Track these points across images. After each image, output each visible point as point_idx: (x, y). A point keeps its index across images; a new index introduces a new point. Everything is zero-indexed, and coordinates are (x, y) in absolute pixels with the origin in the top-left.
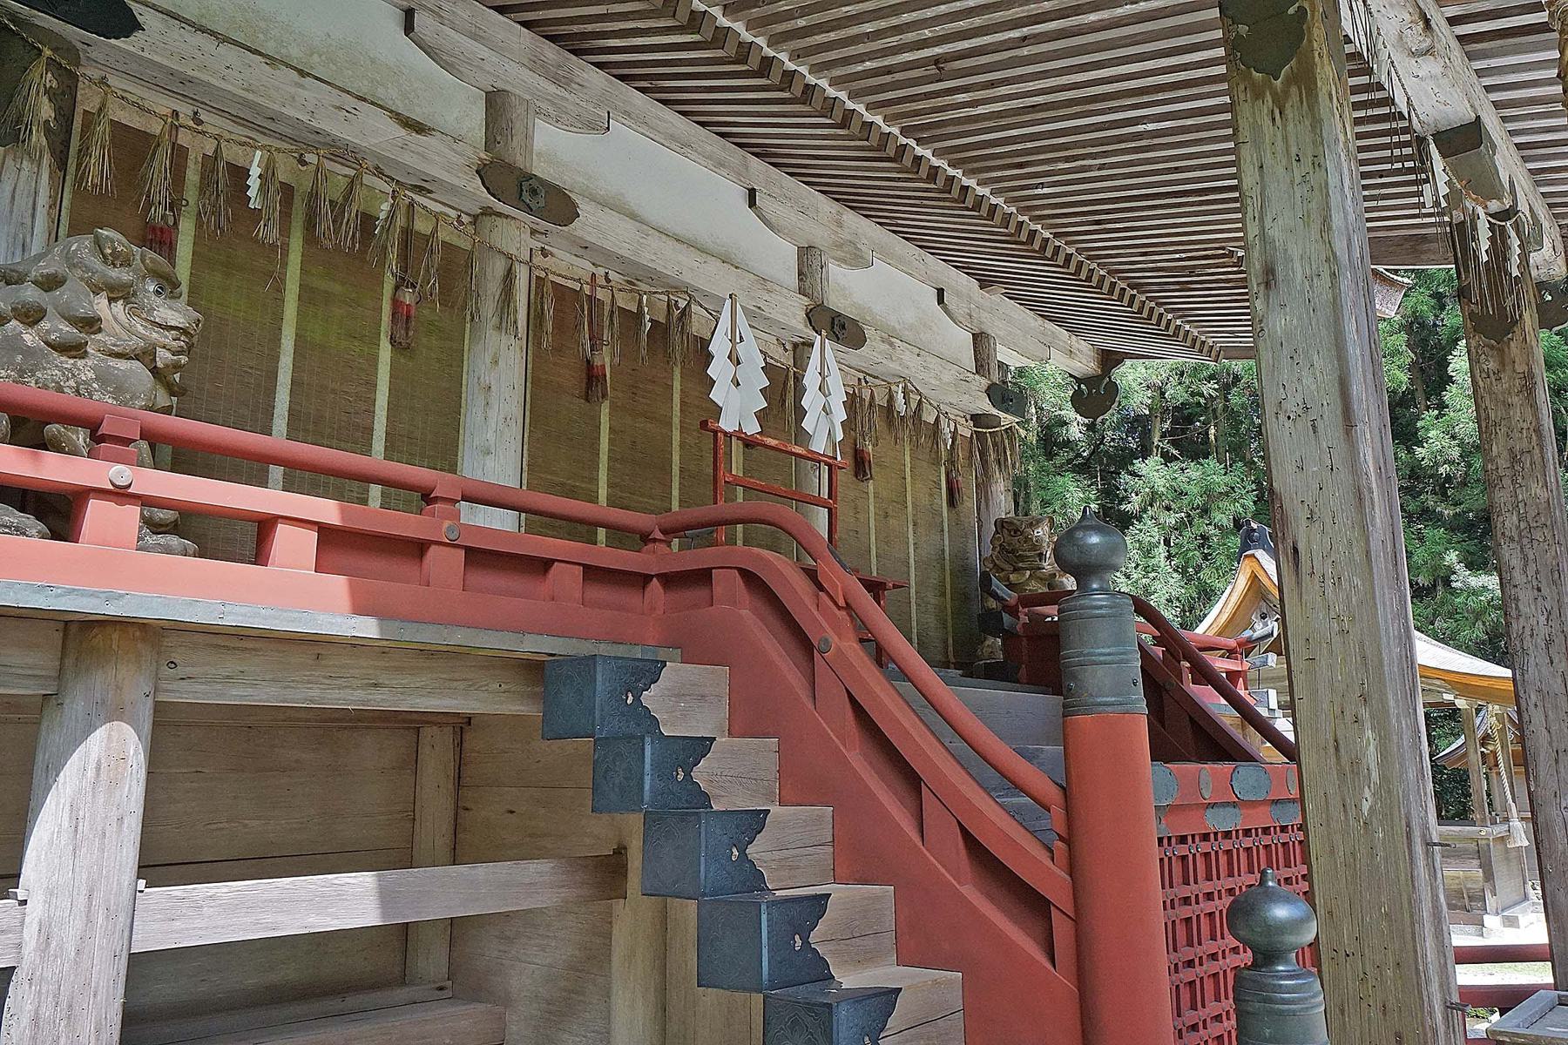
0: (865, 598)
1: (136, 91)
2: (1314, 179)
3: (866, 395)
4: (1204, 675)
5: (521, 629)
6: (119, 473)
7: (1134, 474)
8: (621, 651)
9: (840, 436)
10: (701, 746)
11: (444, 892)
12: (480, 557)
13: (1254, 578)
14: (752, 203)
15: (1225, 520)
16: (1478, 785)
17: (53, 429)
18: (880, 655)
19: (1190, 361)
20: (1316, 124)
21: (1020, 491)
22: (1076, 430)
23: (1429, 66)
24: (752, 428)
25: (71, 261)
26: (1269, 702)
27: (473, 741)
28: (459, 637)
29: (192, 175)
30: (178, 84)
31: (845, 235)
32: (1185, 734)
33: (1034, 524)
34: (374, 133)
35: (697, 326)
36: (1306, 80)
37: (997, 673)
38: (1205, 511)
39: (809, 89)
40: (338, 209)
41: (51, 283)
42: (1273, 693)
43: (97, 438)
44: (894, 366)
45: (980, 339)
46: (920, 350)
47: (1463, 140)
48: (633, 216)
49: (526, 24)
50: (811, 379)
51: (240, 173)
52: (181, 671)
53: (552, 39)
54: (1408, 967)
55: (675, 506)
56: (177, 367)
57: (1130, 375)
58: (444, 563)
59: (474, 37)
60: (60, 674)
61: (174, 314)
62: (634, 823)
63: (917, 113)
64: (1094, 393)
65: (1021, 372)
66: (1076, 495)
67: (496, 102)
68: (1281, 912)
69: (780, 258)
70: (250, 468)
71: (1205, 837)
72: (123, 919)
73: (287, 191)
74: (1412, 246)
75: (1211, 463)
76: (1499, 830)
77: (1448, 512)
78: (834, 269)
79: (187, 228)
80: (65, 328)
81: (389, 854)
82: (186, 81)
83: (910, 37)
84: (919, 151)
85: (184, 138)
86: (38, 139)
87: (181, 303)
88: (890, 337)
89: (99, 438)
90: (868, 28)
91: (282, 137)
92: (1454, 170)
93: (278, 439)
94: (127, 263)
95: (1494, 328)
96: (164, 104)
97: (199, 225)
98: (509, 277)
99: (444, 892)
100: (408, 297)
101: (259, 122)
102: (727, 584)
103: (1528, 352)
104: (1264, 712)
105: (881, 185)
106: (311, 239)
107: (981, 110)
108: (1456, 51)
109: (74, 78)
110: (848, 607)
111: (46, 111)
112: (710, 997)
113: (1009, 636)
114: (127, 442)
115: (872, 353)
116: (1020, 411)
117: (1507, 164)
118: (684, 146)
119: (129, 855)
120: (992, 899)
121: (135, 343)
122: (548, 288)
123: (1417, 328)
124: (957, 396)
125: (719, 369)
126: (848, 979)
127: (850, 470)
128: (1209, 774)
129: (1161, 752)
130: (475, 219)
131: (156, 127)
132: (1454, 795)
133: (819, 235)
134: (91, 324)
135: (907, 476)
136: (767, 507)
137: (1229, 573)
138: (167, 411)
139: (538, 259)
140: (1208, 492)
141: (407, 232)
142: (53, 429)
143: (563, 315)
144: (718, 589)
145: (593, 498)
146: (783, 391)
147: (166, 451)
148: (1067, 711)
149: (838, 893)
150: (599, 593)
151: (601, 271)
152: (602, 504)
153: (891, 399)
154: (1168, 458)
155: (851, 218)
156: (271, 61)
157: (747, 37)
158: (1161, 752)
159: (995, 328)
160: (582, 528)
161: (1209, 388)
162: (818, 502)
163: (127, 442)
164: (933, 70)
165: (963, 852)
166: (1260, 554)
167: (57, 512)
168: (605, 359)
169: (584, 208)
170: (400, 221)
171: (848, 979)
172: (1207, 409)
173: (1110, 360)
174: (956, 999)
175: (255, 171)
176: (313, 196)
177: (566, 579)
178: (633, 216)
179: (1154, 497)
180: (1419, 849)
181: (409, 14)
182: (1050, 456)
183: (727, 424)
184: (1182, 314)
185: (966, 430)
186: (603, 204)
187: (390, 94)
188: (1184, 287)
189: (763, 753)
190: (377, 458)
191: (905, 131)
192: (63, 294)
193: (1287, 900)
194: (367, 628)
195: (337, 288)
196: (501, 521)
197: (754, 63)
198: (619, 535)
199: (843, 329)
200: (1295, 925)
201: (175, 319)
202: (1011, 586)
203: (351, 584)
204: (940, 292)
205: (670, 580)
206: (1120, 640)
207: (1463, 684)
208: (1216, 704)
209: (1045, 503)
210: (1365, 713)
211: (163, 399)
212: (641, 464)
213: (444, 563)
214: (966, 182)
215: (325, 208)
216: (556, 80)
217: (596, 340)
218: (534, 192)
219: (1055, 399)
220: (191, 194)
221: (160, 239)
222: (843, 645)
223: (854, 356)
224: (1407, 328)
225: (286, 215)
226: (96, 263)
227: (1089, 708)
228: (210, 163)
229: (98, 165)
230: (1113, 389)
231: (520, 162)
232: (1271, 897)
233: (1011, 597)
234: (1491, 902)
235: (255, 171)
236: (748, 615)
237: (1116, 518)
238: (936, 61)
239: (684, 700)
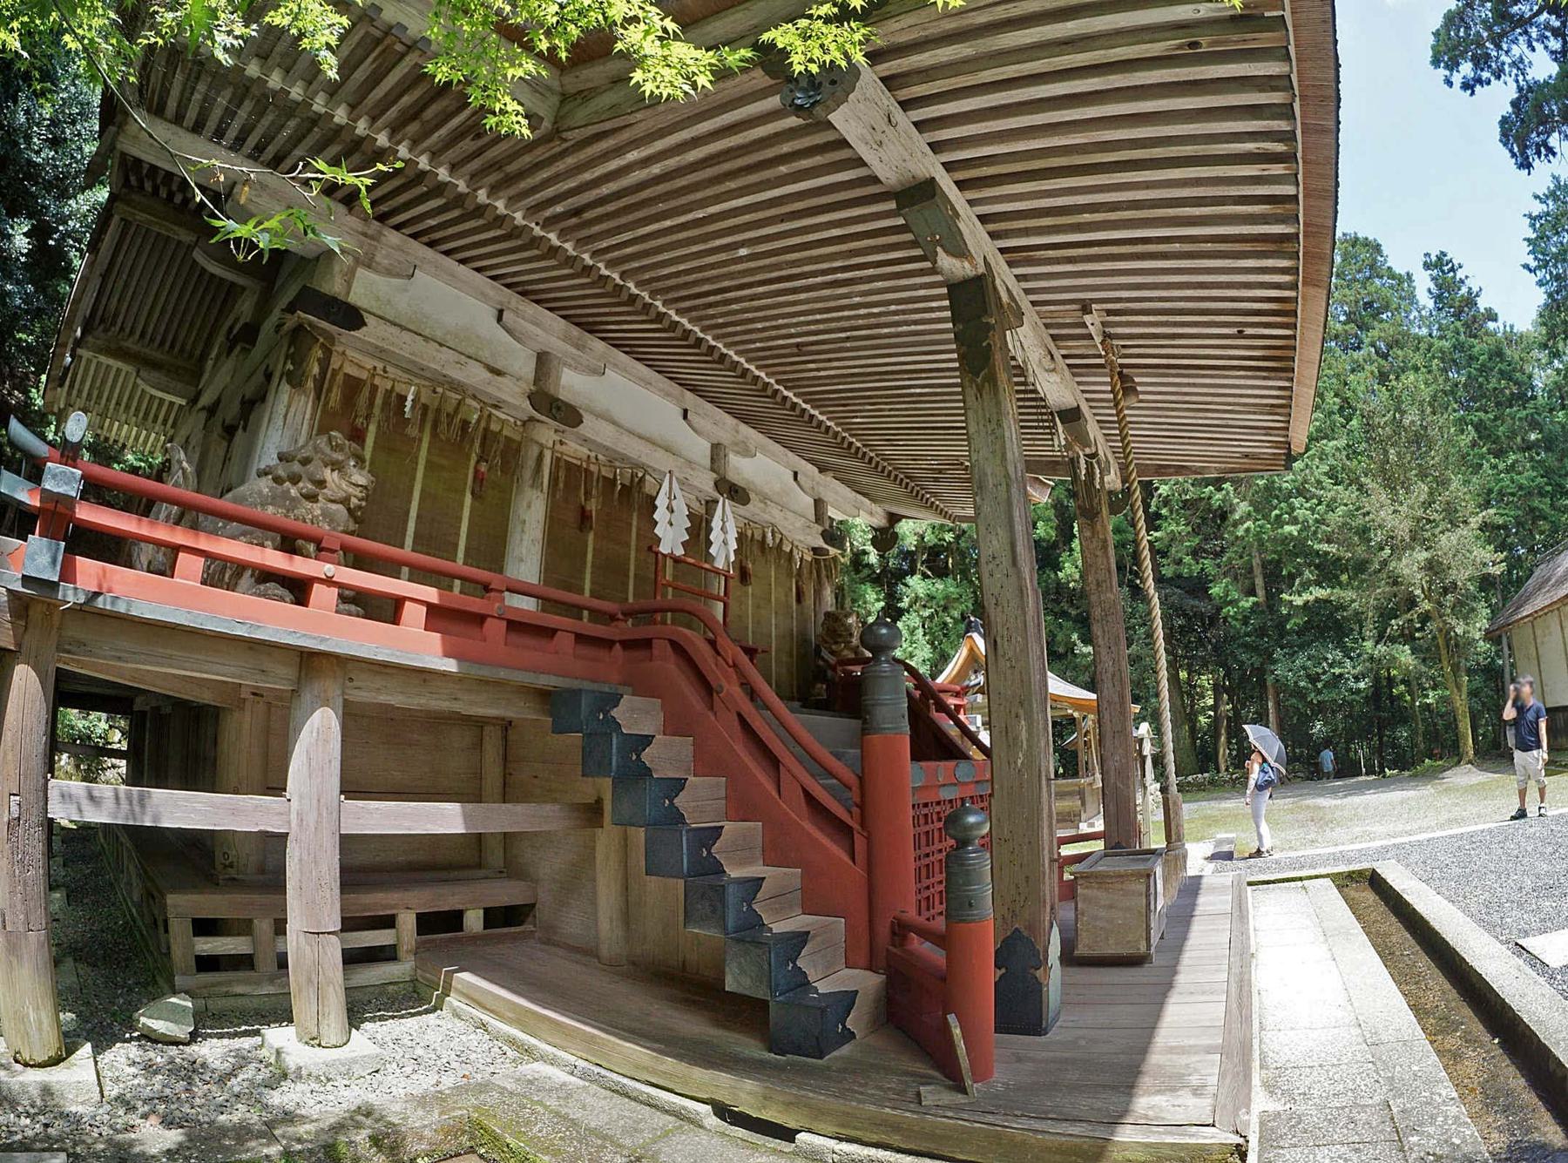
0: (744, 659)
1: (358, 356)
2: (998, 432)
3: (749, 533)
4: (941, 707)
5: (537, 670)
6: (328, 569)
7: (906, 585)
8: (595, 687)
9: (732, 558)
10: (647, 740)
11: (500, 818)
12: (516, 626)
13: (971, 650)
14: (685, 417)
15: (956, 614)
16: (1082, 758)
17: (300, 542)
18: (753, 694)
19: (938, 521)
20: (998, 403)
21: (839, 594)
22: (873, 558)
23: (1054, 378)
24: (680, 552)
25: (316, 449)
26: (976, 722)
27: (512, 736)
28: (503, 674)
29: (379, 401)
30: (379, 353)
31: (740, 437)
32: (933, 744)
33: (847, 616)
34: (474, 375)
35: (649, 488)
36: (992, 380)
37: (822, 706)
38: (945, 609)
39: (723, 356)
40: (450, 417)
41: (305, 462)
42: (979, 718)
43: (319, 549)
44: (767, 517)
45: (819, 504)
46: (783, 507)
47: (1071, 416)
48: (614, 423)
49: (563, 317)
50: (716, 523)
51: (403, 399)
52: (355, 683)
53: (577, 324)
54: (1034, 845)
55: (631, 600)
56: (360, 507)
57: (906, 528)
58: (495, 628)
59: (537, 325)
60: (299, 678)
61: (361, 478)
62: (606, 784)
63: (785, 373)
64: (885, 537)
65: (841, 522)
66: (873, 601)
67: (542, 359)
68: (972, 819)
69: (700, 449)
70: (389, 567)
71: (938, 803)
72: (335, 815)
73: (425, 408)
74: (1051, 466)
75: (950, 580)
76: (1089, 780)
77: (1074, 613)
78: (731, 456)
79: (372, 428)
80: (310, 486)
81: (467, 794)
82: (382, 350)
83: (784, 332)
84: (786, 393)
85: (377, 381)
86: (310, 384)
87: (365, 472)
88: (765, 499)
89: (322, 550)
90: (759, 326)
91: (426, 379)
92: (1067, 431)
93: (407, 552)
94: (342, 450)
95: (1091, 515)
96: (369, 363)
97: (379, 427)
98: (540, 457)
99: (500, 818)
100: (483, 467)
101: (415, 371)
102: (661, 648)
103: (1104, 527)
104: (973, 728)
105: (762, 411)
106: (434, 435)
107: (822, 373)
108: (1067, 371)
109: (331, 352)
110: (735, 665)
111: (316, 370)
112: (653, 882)
113: (831, 685)
114: (333, 551)
115: (754, 509)
116: (841, 547)
117: (1093, 431)
118: (647, 384)
119: (335, 782)
121: (341, 494)
122: (562, 464)
123: (1058, 506)
124: (803, 537)
125: (660, 515)
126: (734, 873)
127: (737, 579)
128: (943, 768)
129: (916, 757)
130: (524, 423)
131: (364, 375)
132: (1070, 763)
133: (725, 437)
134: (321, 484)
135: (773, 585)
136: (689, 602)
137: (956, 648)
138: (352, 533)
139: (558, 447)
140: (947, 597)
141: (486, 429)
142: (300, 542)
143: (570, 479)
144: (655, 652)
145: (581, 591)
146: (699, 528)
147: (351, 557)
148: (865, 731)
149: (728, 826)
150: (585, 651)
151: (593, 454)
152: (586, 597)
153: (764, 536)
154: (925, 576)
155: (744, 428)
156: (426, 339)
157: (689, 326)
158: (916, 757)
159: (827, 496)
160: (575, 610)
161: (949, 537)
162: (718, 599)
163: (333, 551)
164: (795, 350)
165: (804, 804)
166: (975, 636)
167: (299, 589)
168: (593, 506)
169: (587, 418)
170: (483, 424)
171: (734, 873)
172: (948, 548)
173: (894, 518)
174: (797, 883)
175: (410, 397)
176: (438, 411)
177: (565, 642)
178: (614, 423)
179: (917, 599)
180: (1044, 782)
181: (501, 312)
182: (857, 572)
183: (664, 549)
184: (934, 494)
185: (808, 557)
186: (599, 416)
187: (485, 355)
188: (936, 480)
189: (684, 746)
190: (459, 563)
191: (778, 382)
192: (310, 467)
193: (976, 813)
194: (451, 665)
195: (444, 462)
196: (527, 604)
197: (691, 341)
198: (597, 615)
199: (736, 493)
200: (978, 825)
201: (362, 480)
202: (832, 653)
203: (443, 640)
204: (796, 474)
205: (627, 645)
206: (896, 691)
207: (1077, 704)
208: (949, 726)
209: (854, 601)
210: (1021, 712)
211: (352, 526)
212: (612, 569)
213: (495, 628)
214: (813, 412)
215: (443, 418)
216: (577, 347)
217: (588, 494)
218: (559, 409)
219: (861, 538)
220: (377, 411)
221: (357, 436)
222: (732, 689)
223: (741, 510)
224: (1054, 506)
225: (423, 421)
226: (327, 450)
227: (878, 730)
228: (388, 393)
229: (336, 396)
230: (895, 536)
231: (552, 392)
232: (969, 812)
233: (832, 660)
234: (1083, 816)
235: (410, 397)
236: (667, 666)
237: (893, 612)
238: (798, 345)
239: (635, 715)
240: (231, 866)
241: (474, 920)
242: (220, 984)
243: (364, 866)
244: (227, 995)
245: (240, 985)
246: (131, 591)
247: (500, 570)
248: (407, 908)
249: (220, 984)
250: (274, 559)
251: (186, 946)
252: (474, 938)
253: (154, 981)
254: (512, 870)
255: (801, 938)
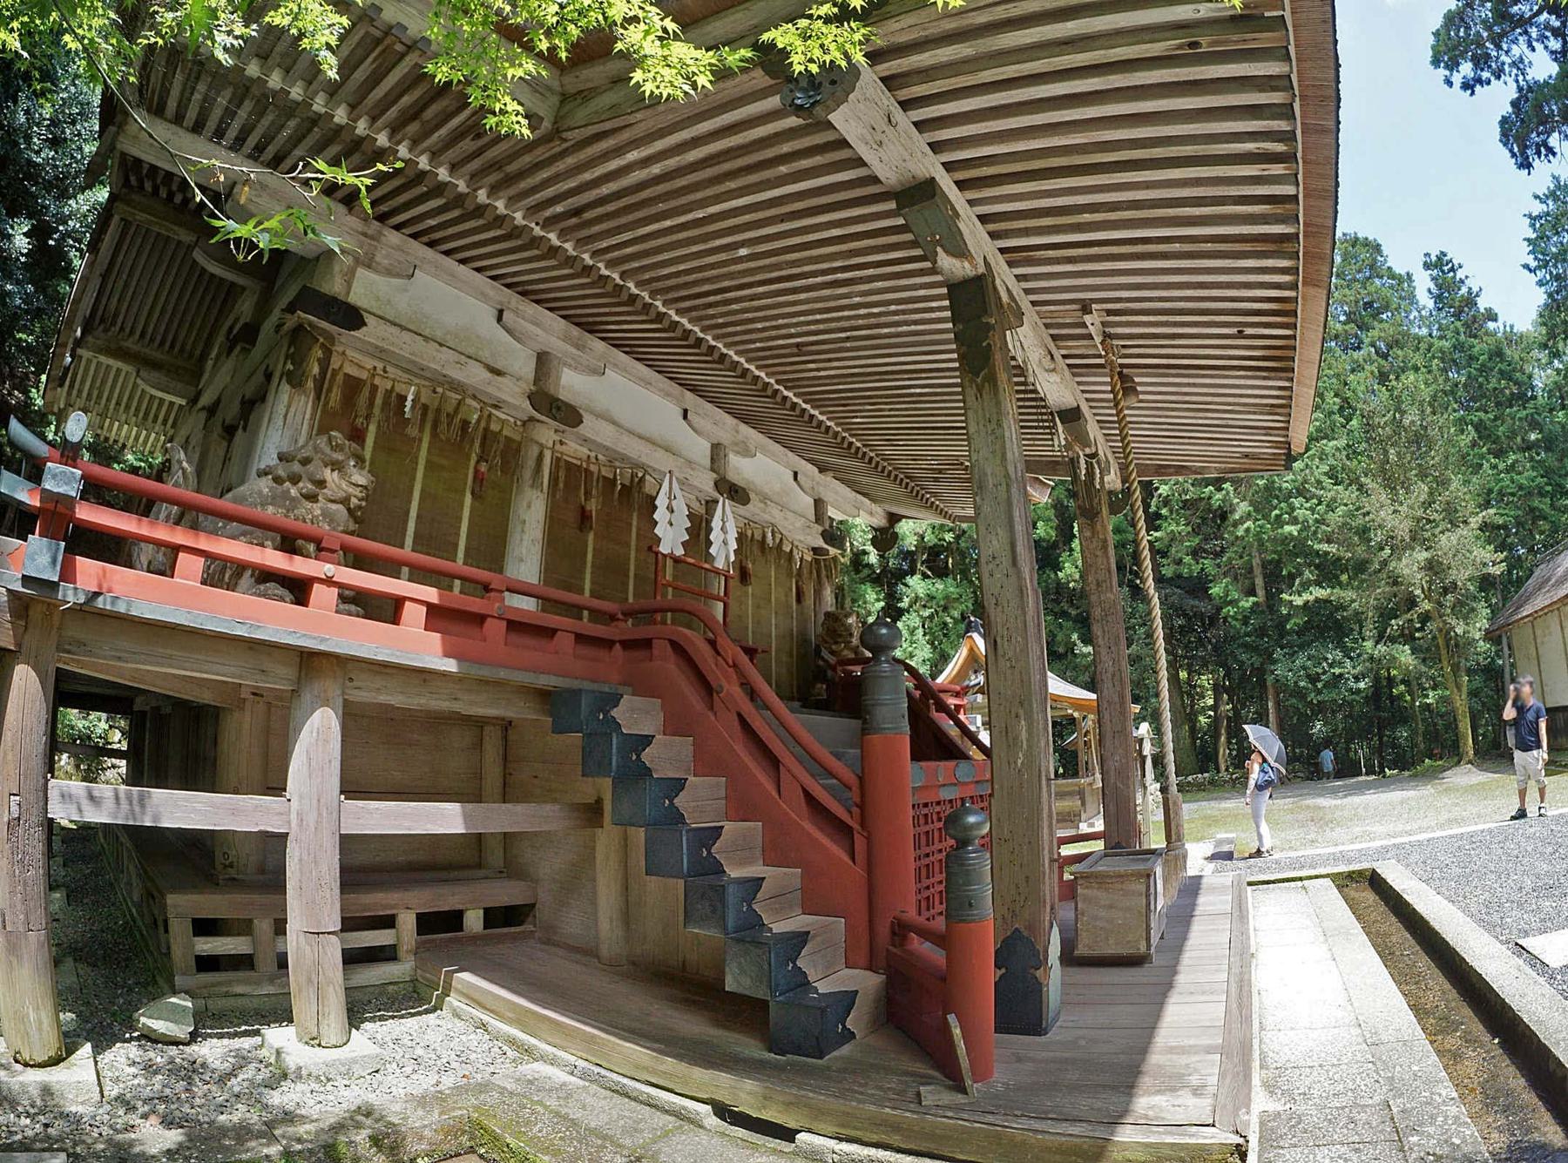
0: (744, 659)
1: (358, 356)
2: (998, 432)
3: (749, 533)
4: (941, 707)
5: (537, 670)
6: (328, 569)
7: (906, 585)
8: (595, 687)
9: (732, 558)
10: (647, 740)
11: (500, 818)
12: (516, 626)
13: (971, 650)
14: (685, 417)
15: (956, 614)
16: (1082, 758)
17: (300, 542)
18: (753, 694)
19: (938, 521)
20: (998, 403)
21: (839, 594)
22: (873, 558)
23: (1054, 378)
24: (680, 552)
25: (316, 449)
27: (512, 736)
28: (503, 674)
29: (379, 401)
30: (379, 353)
31: (740, 437)
32: (933, 744)
33: (847, 616)
34: (474, 375)
35: (649, 488)
36: (992, 380)
37: (822, 706)
38: (945, 609)
39: (723, 356)
40: (450, 417)
41: (305, 462)
43: (319, 549)
44: (767, 517)
45: (819, 504)
46: (783, 507)
47: (1071, 416)
48: (614, 423)
49: (563, 317)
50: (716, 523)
51: (403, 399)
52: (355, 683)
53: (577, 324)
54: (1034, 845)
55: (631, 600)
56: (360, 507)
57: (906, 528)
58: (495, 628)
59: (537, 325)
60: (299, 678)
61: (361, 478)
62: (606, 784)
63: (785, 373)
64: (885, 537)
65: (841, 522)
66: (873, 601)
67: (542, 359)
68: (972, 819)
69: (700, 449)
70: (389, 567)
72: (335, 815)
73: (425, 408)
74: (1051, 466)
75: (950, 580)
76: (1089, 780)
77: (1074, 613)
78: (731, 456)
79: (372, 428)
80: (310, 486)
81: (467, 794)
82: (382, 350)
83: (784, 332)
84: (786, 393)
85: (377, 381)
86: (310, 384)
87: (365, 472)
88: (765, 499)
89: (322, 550)
90: (759, 326)
91: (426, 379)
92: (1067, 431)
93: (407, 552)
94: (342, 450)
95: (1091, 515)
96: (369, 363)
97: (379, 427)
98: (540, 457)
99: (500, 818)
100: (483, 467)
101: (415, 371)
102: (661, 648)
103: (1104, 527)
105: (762, 411)
106: (434, 435)
107: (822, 373)
108: (1067, 371)
109: (331, 352)
110: (735, 665)
111: (316, 370)
112: (653, 882)
113: (831, 685)
114: (333, 551)
115: (754, 509)
116: (841, 547)
117: (1093, 431)
118: (647, 384)
119: (335, 782)
120: (821, 830)
121: (341, 494)
122: (562, 464)
123: (1058, 506)
124: (803, 537)
125: (660, 515)
126: (734, 873)
127: (737, 579)
130: (524, 423)
131: (364, 375)
132: (1070, 763)
133: (725, 437)
134: (321, 484)
135: (773, 585)
136: (689, 602)
137: (956, 648)
138: (352, 533)
139: (558, 447)
140: (947, 597)
141: (486, 429)
142: (300, 542)
143: (570, 479)
144: (655, 652)
145: (581, 591)
146: (699, 528)
147: (351, 557)
148: (865, 731)
149: (728, 826)
150: (585, 651)
151: (593, 454)
152: (586, 597)
153: (764, 536)
154: (925, 576)
155: (744, 428)
156: (426, 339)
157: (689, 326)
159: (827, 496)
160: (575, 610)
161: (949, 537)
162: (718, 599)
163: (333, 551)
164: (795, 350)
165: (804, 804)
166: (975, 636)
167: (299, 589)
168: (593, 506)
169: (587, 418)
170: (483, 424)
171: (734, 873)
172: (948, 548)
173: (894, 518)
174: (797, 883)
175: (410, 397)
176: (438, 411)
177: (565, 642)
178: (614, 423)
179: (917, 599)
180: (1044, 782)
181: (501, 312)
182: (857, 572)
183: (664, 549)
184: (934, 494)
185: (808, 557)
186: (599, 416)
187: (485, 355)
188: (936, 480)
189: (684, 746)
190: (459, 563)
191: (778, 382)
192: (310, 467)
193: (976, 813)
194: (451, 665)
195: (444, 462)
196: (527, 604)
197: (691, 341)
198: (597, 615)
199: (736, 493)
200: (978, 825)
201: (362, 480)
202: (832, 653)
203: (443, 640)
204: (796, 474)
205: (627, 645)
206: (896, 691)
207: (1077, 704)
208: (949, 726)
209: (854, 601)
210: (1021, 712)
211: (352, 526)
212: (612, 569)
213: (495, 628)
214: (813, 412)
215: (443, 418)
216: (577, 347)
217: (588, 494)
218: (559, 409)
219: (861, 538)
220: (377, 411)
221: (357, 436)
222: (732, 689)
223: (741, 510)
224: (1054, 506)
225: (423, 421)
226: (327, 450)
227: (878, 730)
228: (388, 393)
229: (336, 396)
230: (895, 536)
231: (552, 392)
232: (969, 812)
233: (832, 660)
234: (1083, 816)
235: (410, 397)
236: (667, 666)
237: (893, 612)
238: (798, 345)
239: (635, 715)
240: (231, 866)
241: (474, 920)
242: (220, 984)
243: (364, 866)
244: (227, 995)
245: (240, 985)
246: (131, 591)
247: (500, 570)
248: (407, 908)
249: (220, 984)
250: (274, 559)
251: (186, 946)
252: (474, 938)
253: (154, 981)
254: (512, 870)
255: (801, 938)
